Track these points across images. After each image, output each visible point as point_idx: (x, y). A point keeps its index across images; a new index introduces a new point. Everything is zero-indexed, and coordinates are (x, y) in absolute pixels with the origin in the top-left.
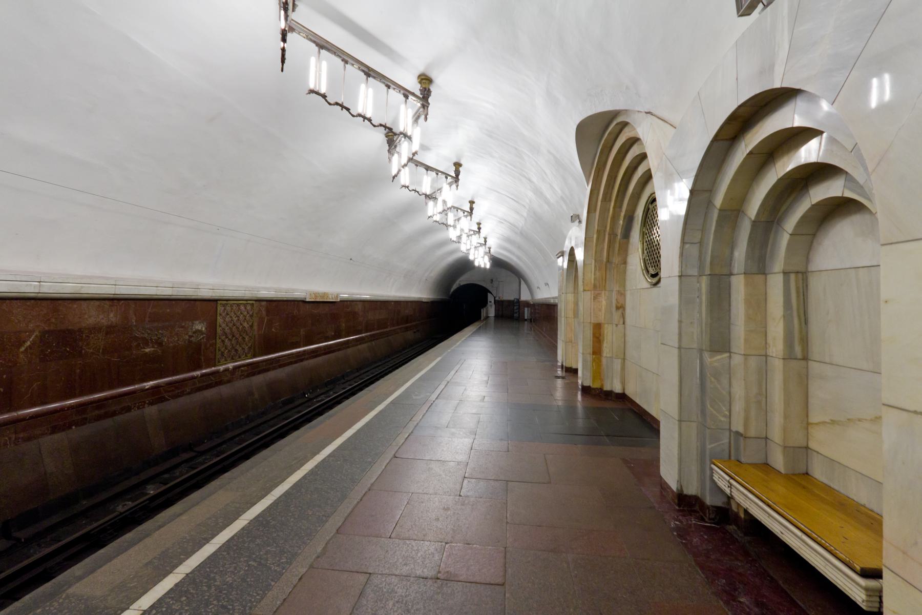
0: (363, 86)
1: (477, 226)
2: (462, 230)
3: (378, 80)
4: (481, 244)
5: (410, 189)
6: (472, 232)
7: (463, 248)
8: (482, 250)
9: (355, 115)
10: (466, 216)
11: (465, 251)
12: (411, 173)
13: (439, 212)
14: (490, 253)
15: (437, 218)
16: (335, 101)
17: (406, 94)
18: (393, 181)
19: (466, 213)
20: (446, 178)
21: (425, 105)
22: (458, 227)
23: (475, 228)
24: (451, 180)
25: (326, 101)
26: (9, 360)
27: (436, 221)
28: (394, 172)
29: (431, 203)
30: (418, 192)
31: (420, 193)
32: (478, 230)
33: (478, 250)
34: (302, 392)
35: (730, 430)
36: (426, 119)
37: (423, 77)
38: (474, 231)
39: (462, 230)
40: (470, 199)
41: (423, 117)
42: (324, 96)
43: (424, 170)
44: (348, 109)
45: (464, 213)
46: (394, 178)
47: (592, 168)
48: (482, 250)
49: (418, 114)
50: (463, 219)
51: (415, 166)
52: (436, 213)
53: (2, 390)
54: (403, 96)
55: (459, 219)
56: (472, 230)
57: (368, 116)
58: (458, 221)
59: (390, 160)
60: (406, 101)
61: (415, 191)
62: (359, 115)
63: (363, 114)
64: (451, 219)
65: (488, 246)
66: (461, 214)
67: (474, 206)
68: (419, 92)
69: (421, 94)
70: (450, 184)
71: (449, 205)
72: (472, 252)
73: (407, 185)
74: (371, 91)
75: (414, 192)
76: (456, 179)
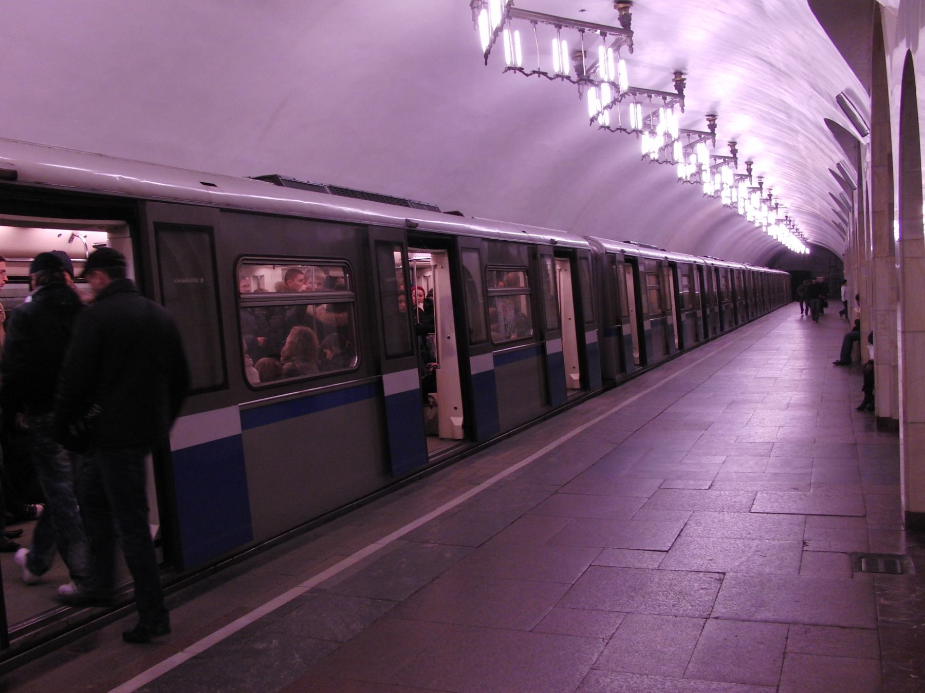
1: (729, 149)
2: (667, 135)
3: (570, 28)
5: (660, 162)
9: (529, 73)
11: (713, 194)
13: (605, 104)
15: (605, 119)
19: (669, 99)
22: (660, 129)
28: (485, 44)
31: (550, 75)
32: (731, 155)
33: (720, 173)
36: (632, 51)
38: (724, 158)
40: (746, 160)
45: (665, 99)
46: (486, 55)
51: (532, 25)
53: (219, 692)
56: (720, 157)
59: (475, 20)
60: (604, 39)
61: (539, 73)
63: (560, 74)
64: (635, 115)
65: (742, 157)
67: (737, 147)
72: (740, 205)
75: (619, 131)
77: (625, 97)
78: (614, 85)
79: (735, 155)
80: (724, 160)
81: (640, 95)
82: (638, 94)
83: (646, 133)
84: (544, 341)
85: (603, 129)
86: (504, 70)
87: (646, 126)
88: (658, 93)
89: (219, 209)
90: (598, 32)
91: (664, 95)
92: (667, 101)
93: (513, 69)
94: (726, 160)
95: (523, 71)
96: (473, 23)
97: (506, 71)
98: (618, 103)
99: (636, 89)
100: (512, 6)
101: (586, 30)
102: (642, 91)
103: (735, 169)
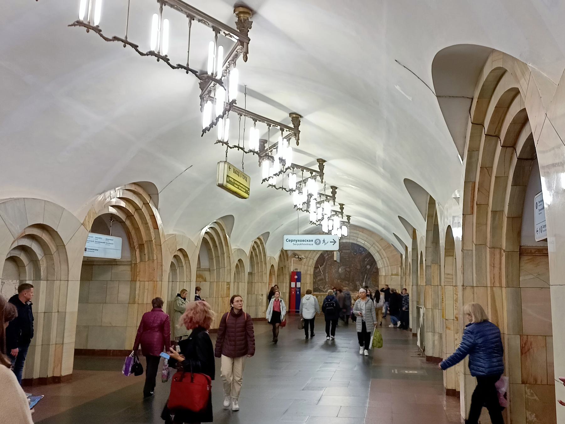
0: (155, 17)
4: (336, 212)
5: (303, 210)
6: (323, 198)
7: (313, 217)
8: (337, 220)
9: (247, 151)
10: (314, 178)
12: (232, 126)
14: (349, 222)
16: (113, 35)
17: (217, 26)
18: (215, 144)
20: (282, 130)
21: (244, 41)
22: (305, 190)
23: (338, 208)
24: (288, 133)
25: (101, 35)
26: (379, 342)
27: (272, 186)
28: (206, 124)
29: (266, 163)
30: (285, 189)
31: (246, 150)
32: (340, 211)
34: (235, 407)
35: (439, 333)
36: (246, 59)
37: (241, 9)
38: (327, 196)
39: (310, 196)
41: (241, 56)
42: (97, 30)
43: (250, 121)
44: (135, 47)
45: (312, 173)
46: (204, 131)
47: (438, 270)
48: (337, 220)
49: (235, 52)
50: (311, 182)
52: (272, 175)
54: (212, 29)
55: (305, 181)
57: (163, 54)
58: (305, 183)
62: (151, 53)
63: (156, 52)
65: (338, 200)
66: (307, 174)
68: (236, 26)
69: (237, 28)
70: (288, 138)
71: (288, 164)
73: (225, 141)
74: (166, 22)
76: (296, 132)
77: (265, 182)
78: (282, 161)
79: (342, 211)
80: (336, 213)
81: (297, 169)
82: (295, 168)
83: (297, 191)
84: (191, 372)
85: (271, 187)
86: (216, 142)
87: (297, 188)
88: (308, 169)
89: (270, 168)
90: (279, 127)
91: (312, 171)
92: (312, 175)
93: (237, 147)
94: (337, 213)
95: (101, 33)
96: (201, 106)
97: (217, 143)
98: (267, 181)
99: (295, 165)
100: (234, 104)
101: (305, 170)
102: (298, 167)
103: (342, 218)
